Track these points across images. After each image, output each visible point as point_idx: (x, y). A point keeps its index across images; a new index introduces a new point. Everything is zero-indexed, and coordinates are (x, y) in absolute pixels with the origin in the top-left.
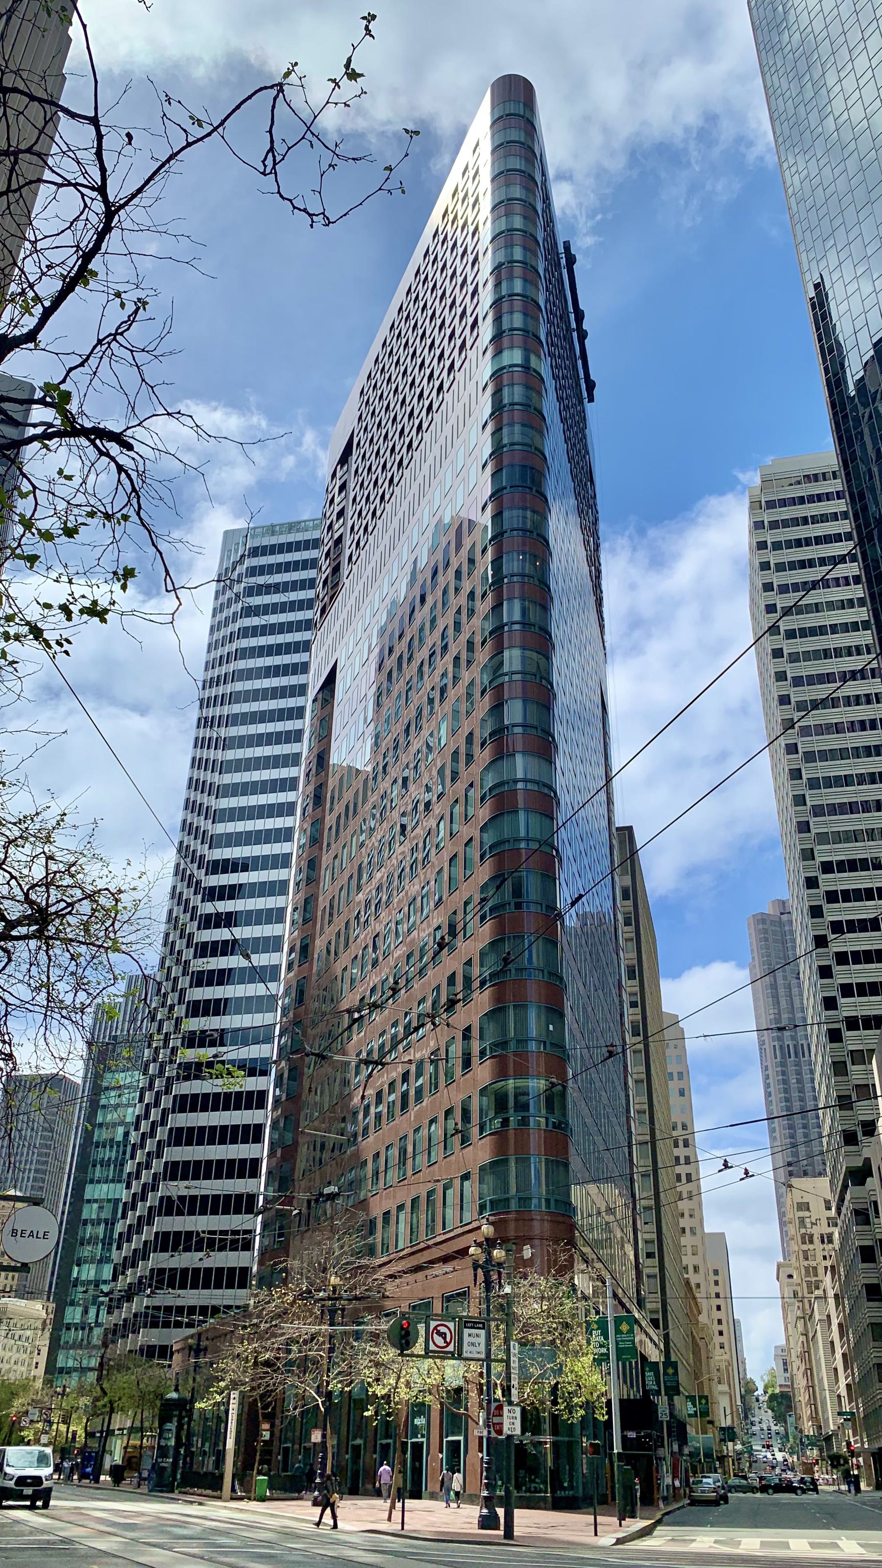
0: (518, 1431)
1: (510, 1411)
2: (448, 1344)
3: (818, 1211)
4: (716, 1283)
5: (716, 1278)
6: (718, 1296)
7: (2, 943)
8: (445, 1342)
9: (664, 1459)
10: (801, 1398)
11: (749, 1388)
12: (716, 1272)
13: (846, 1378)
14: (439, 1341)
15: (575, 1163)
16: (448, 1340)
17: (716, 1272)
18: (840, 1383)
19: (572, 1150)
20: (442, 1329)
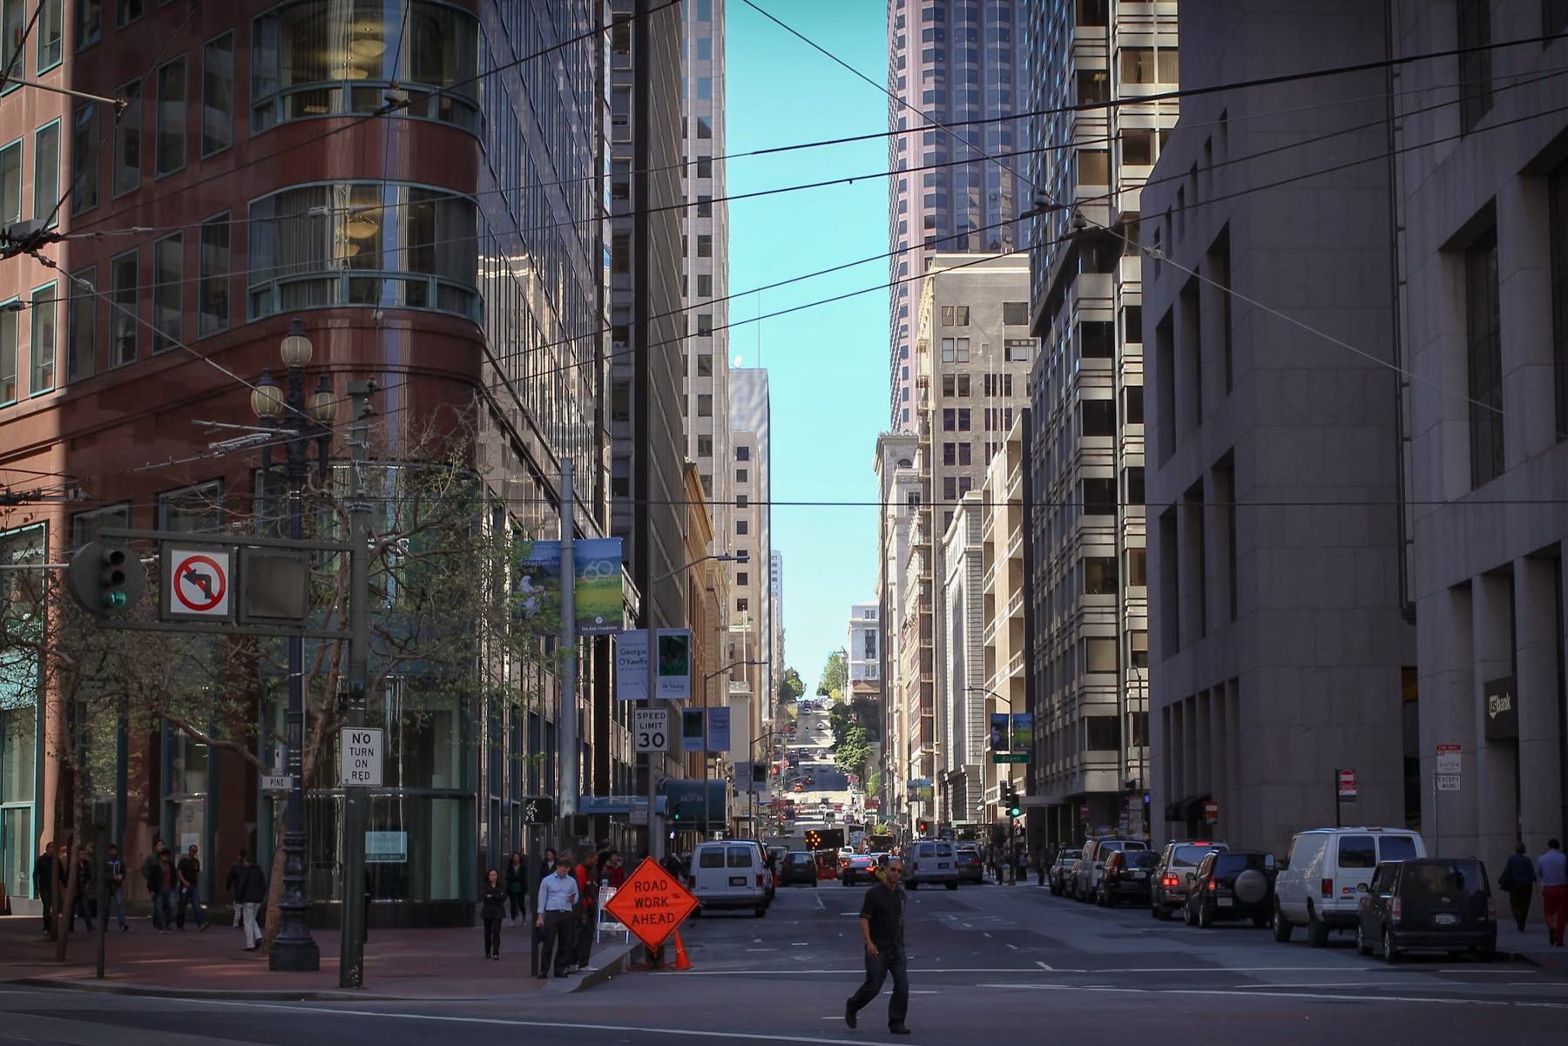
0: (375, 778)
1: (356, 739)
2: (215, 600)
3: (991, 328)
4: (742, 476)
5: (742, 465)
6: (742, 502)
7: (1172, 8)
8: (208, 594)
9: (101, 975)
10: (904, 707)
11: (788, 689)
12: (743, 454)
13: (1012, 666)
14: (195, 594)
15: (489, 209)
16: (215, 589)
17: (743, 454)
18: (997, 676)
19: (483, 180)
20: (201, 568)
